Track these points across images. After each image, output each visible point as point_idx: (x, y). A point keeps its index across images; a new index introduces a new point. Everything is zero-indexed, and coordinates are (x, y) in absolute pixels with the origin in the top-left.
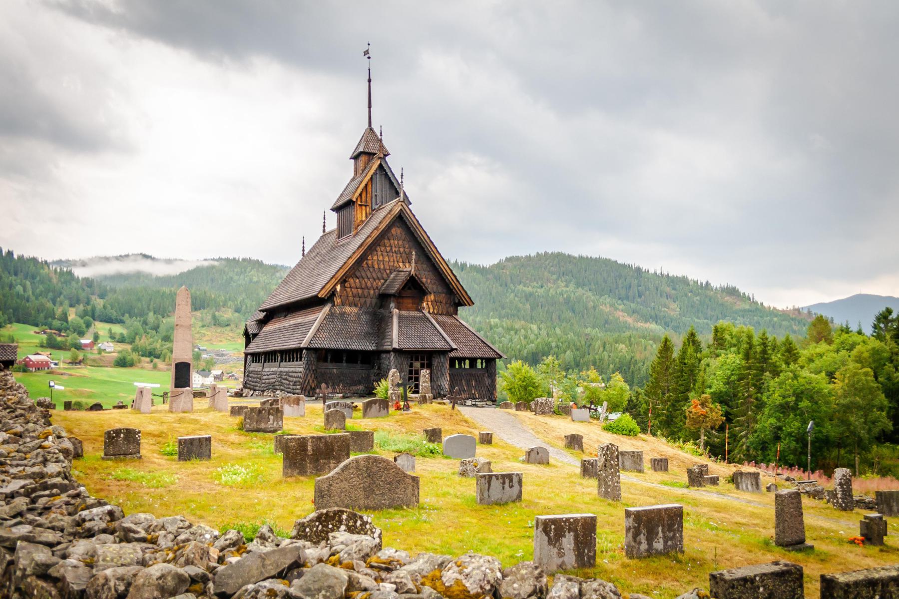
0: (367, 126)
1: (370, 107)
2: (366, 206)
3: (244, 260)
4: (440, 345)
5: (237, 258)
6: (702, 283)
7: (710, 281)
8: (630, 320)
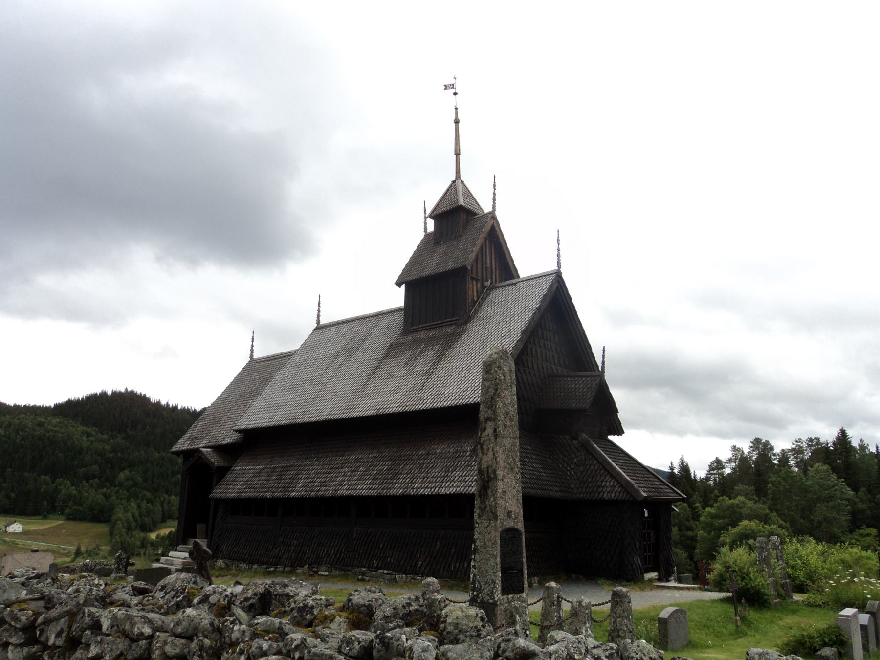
1: (457, 154)
2: (477, 280)
6: (863, 447)
7: (866, 442)
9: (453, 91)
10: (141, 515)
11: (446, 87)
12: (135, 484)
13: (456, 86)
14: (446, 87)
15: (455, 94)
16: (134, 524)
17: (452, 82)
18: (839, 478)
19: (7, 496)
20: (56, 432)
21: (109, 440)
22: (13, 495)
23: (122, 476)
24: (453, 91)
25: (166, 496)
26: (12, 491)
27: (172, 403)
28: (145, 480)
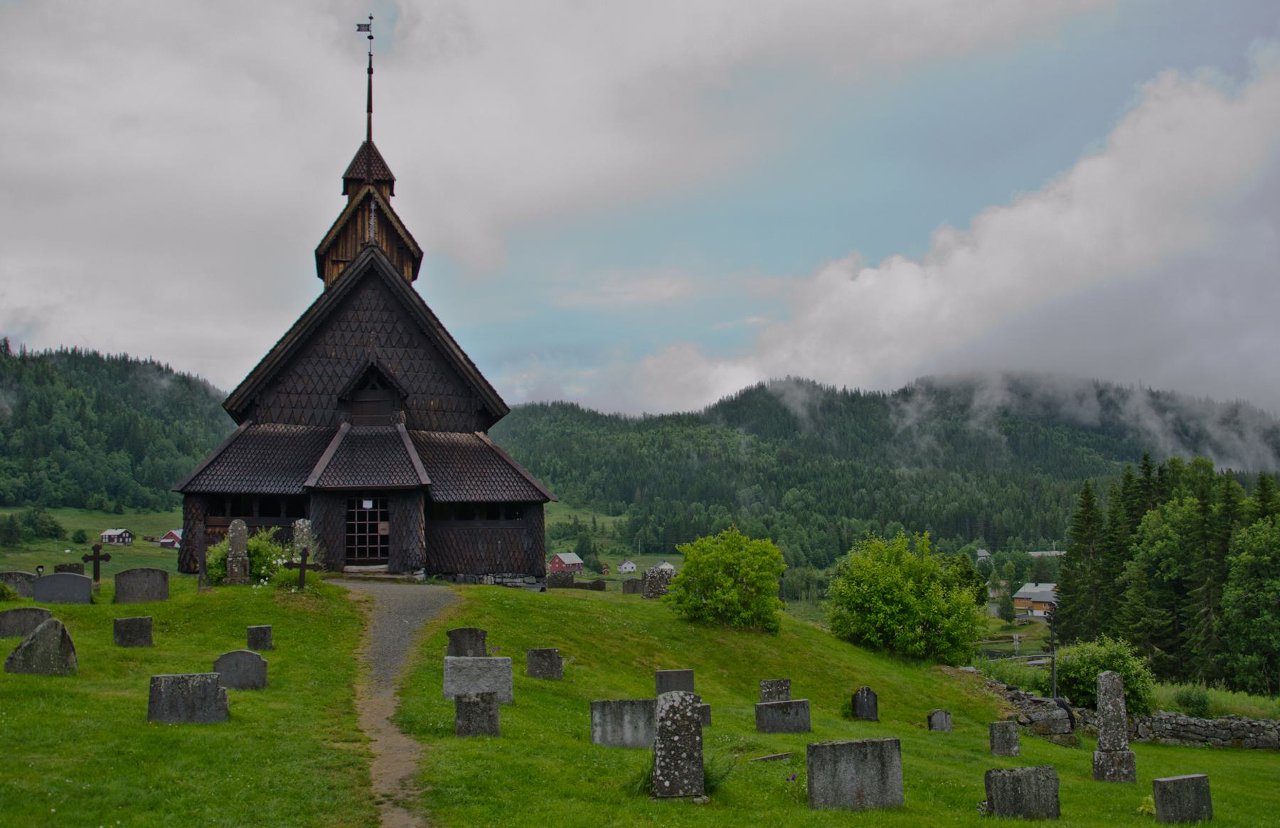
0: (365, 139)
1: (370, 110)
3: (554, 404)
5: (545, 401)
8: (1098, 458)
9: (368, 34)
10: (813, 547)
11: (361, 28)
12: (807, 506)
13: (372, 28)
14: (361, 28)
15: (371, 38)
16: (803, 559)
17: (367, 22)
18: (1155, 507)
19: (656, 532)
20: (708, 445)
21: (774, 449)
22: (661, 529)
23: (788, 496)
24: (368, 34)
25: (845, 519)
26: (660, 524)
27: (851, 388)
28: (819, 499)
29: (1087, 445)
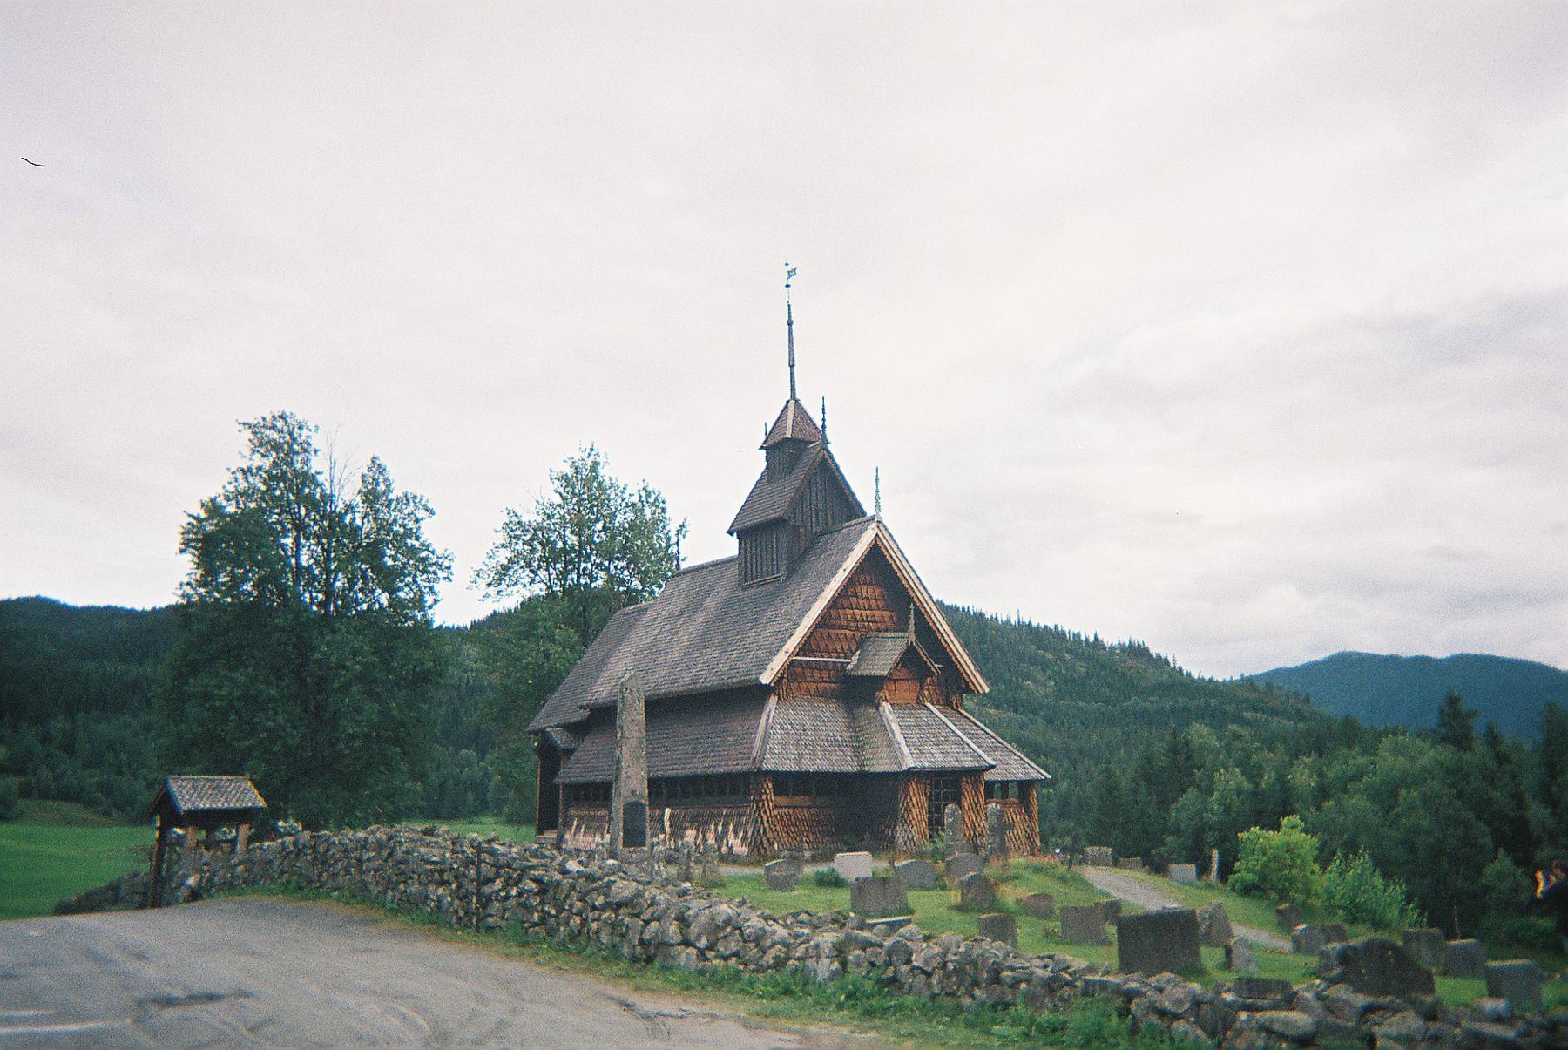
1: (792, 366)
4: (968, 763)
7: (1100, 637)
29: (531, 868)
